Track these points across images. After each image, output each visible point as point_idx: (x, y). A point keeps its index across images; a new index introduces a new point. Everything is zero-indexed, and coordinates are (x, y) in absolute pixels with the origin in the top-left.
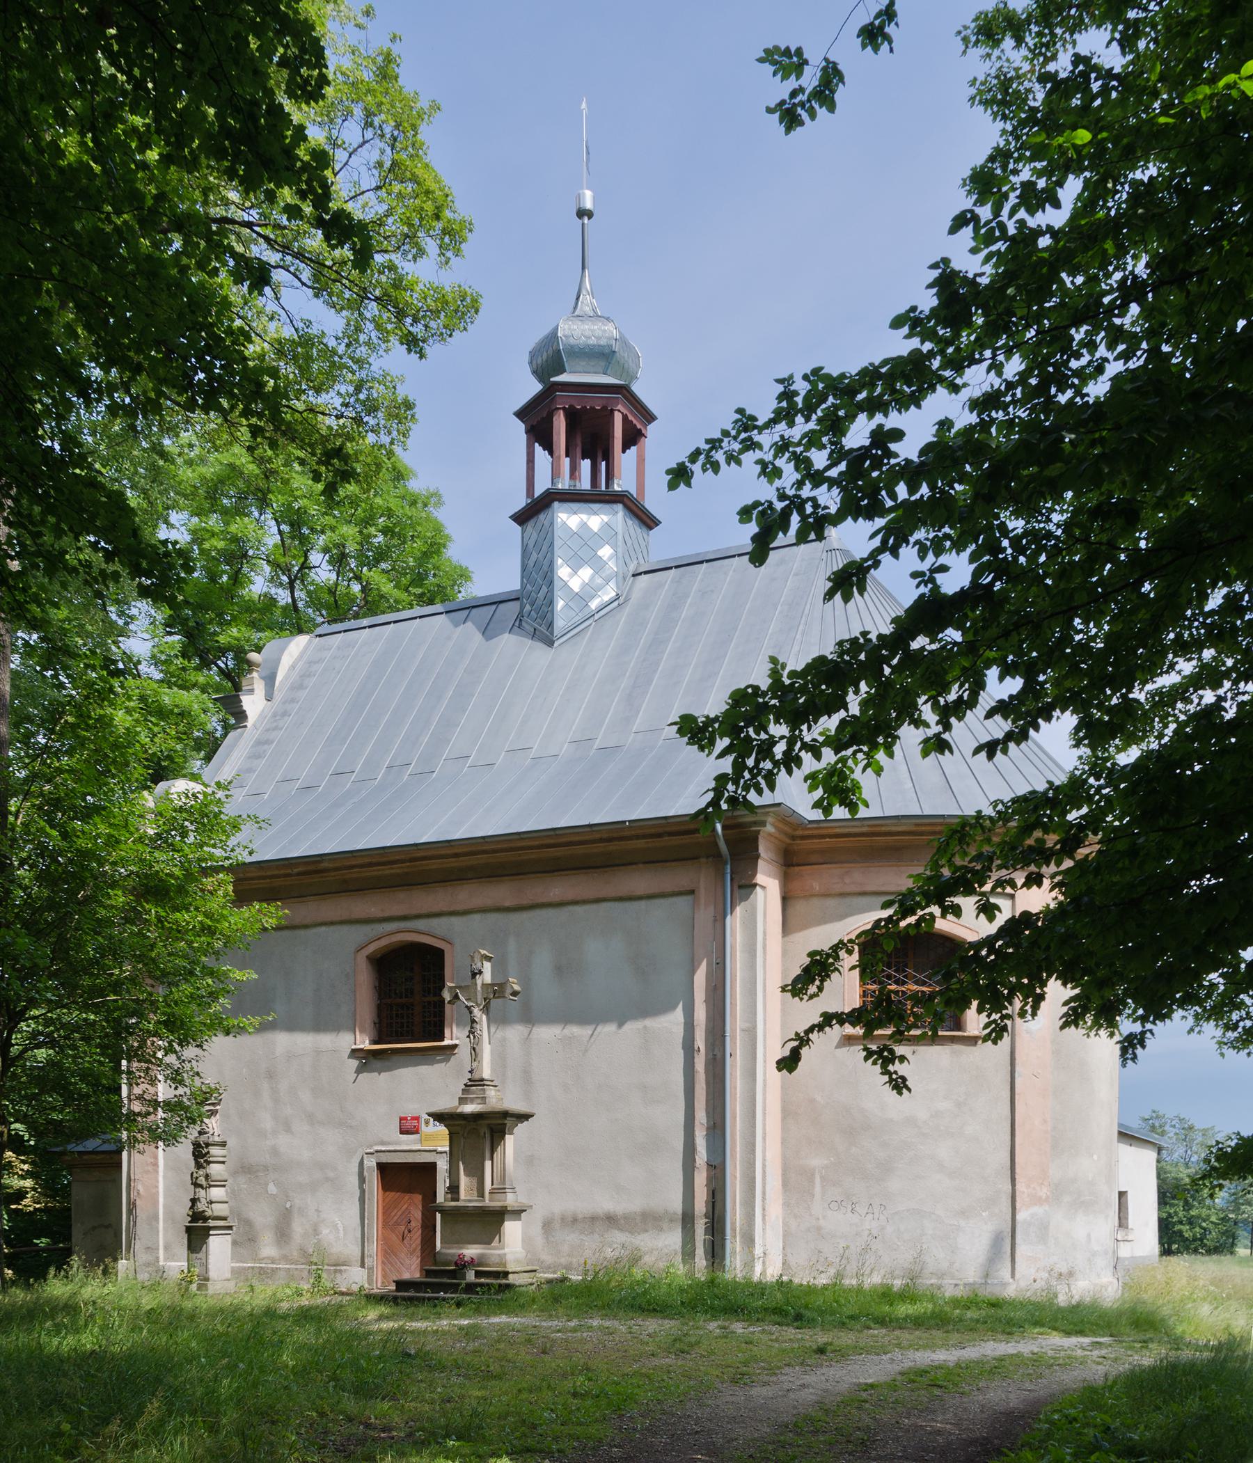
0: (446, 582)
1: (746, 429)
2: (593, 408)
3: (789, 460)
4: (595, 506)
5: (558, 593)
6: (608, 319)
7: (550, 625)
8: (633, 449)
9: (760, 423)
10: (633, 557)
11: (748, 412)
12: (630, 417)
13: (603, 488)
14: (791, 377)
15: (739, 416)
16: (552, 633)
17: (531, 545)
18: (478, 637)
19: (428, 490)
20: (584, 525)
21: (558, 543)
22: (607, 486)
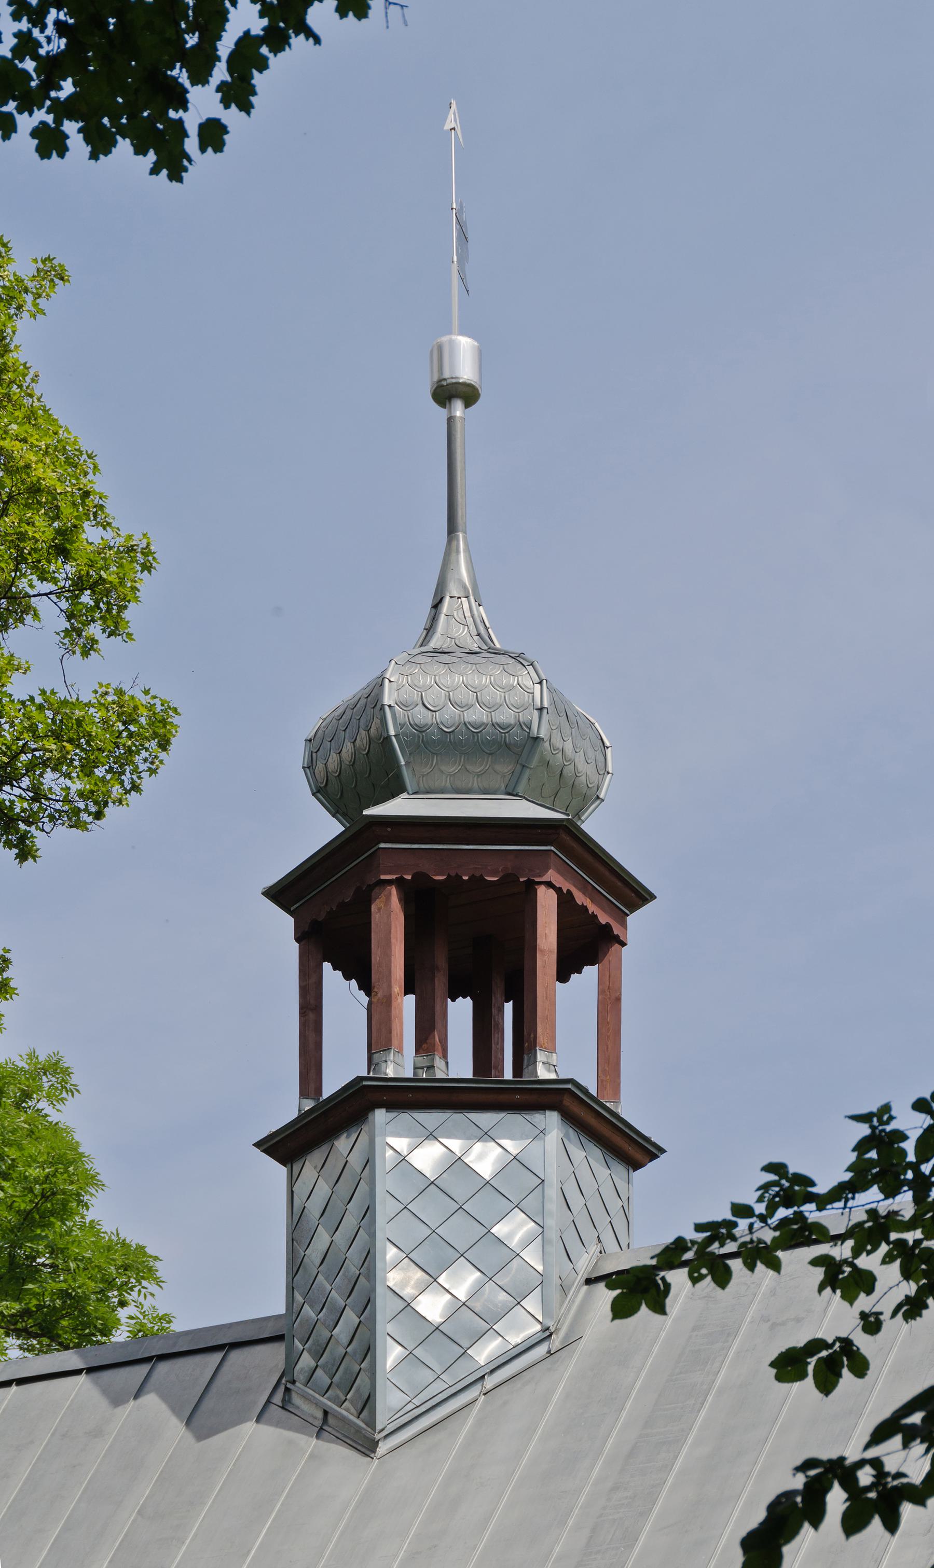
0: (87, 1285)
1: (788, 1199)
2: (477, 880)
3: (887, 1259)
4: (485, 1119)
5: (385, 1326)
6: (518, 658)
7: (367, 1403)
8: (590, 972)
9: (822, 1187)
10: (588, 1234)
11: (792, 1170)
12: (580, 898)
13: (508, 1074)
14: (886, 1108)
15: (772, 1177)
16: (371, 1423)
17: (314, 1207)
18: (175, 1428)
19: (32, 1056)
20: (456, 1163)
21: (384, 1208)
22: (518, 1069)
